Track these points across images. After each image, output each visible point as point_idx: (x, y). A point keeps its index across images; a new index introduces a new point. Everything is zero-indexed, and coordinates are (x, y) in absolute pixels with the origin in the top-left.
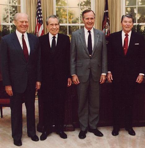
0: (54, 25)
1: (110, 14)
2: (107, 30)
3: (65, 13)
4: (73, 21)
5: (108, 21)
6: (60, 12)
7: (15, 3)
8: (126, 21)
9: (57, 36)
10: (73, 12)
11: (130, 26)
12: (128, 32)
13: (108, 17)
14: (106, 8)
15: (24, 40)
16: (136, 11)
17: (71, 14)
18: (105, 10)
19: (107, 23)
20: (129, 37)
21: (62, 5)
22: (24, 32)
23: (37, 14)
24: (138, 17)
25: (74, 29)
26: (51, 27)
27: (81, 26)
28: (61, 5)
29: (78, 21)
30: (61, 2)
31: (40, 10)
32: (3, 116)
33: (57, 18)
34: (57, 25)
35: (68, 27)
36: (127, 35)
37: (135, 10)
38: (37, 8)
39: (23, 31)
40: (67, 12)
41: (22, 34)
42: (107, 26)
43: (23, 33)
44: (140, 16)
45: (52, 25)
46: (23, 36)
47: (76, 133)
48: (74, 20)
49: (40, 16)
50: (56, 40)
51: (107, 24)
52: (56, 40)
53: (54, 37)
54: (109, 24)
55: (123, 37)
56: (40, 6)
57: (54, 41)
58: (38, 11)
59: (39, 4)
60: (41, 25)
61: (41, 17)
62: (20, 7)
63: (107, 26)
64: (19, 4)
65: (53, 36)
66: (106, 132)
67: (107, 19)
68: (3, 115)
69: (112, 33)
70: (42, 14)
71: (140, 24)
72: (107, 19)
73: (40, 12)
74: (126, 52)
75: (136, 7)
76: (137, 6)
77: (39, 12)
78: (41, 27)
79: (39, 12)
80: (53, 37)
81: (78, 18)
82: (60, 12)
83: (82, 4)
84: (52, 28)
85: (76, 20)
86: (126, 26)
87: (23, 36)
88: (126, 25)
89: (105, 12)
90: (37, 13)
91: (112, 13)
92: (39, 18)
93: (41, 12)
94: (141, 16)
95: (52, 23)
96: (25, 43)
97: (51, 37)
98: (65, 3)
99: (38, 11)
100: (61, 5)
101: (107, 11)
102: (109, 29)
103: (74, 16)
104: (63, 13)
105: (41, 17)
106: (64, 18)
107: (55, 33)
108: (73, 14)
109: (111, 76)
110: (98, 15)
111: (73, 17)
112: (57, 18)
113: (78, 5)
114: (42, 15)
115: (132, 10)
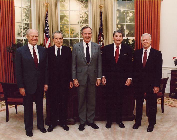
0: (59, 39)
1: (104, 30)
2: (101, 43)
3: (67, 29)
5: (103, 36)
7: (27, 21)
9: (61, 48)
10: (74, 29)
12: (119, 44)
13: (102, 32)
14: (101, 25)
16: (125, 28)
17: (72, 30)
18: (100, 27)
19: (102, 37)
20: (120, 49)
21: (65, 23)
22: (35, 45)
23: (45, 30)
24: (126, 32)
26: (57, 41)
28: (65, 22)
29: (78, 36)
31: (47, 27)
33: (62, 33)
34: (61, 39)
36: (118, 47)
38: (45, 25)
39: (34, 43)
41: (32, 46)
42: (101, 39)
43: (34, 45)
44: (128, 32)
45: (57, 39)
46: (34, 47)
47: (77, 126)
48: (75, 35)
49: (47, 31)
50: (60, 51)
51: (101, 38)
52: (60, 51)
53: (59, 49)
54: (103, 38)
55: (115, 49)
56: (47, 24)
59: (47, 22)
62: (31, 24)
63: (101, 39)
65: (58, 48)
66: (101, 125)
67: (102, 34)
70: (49, 30)
72: (102, 34)
73: (47, 28)
74: (117, 61)
75: (125, 25)
76: (126, 24)
77: (46, 28)
78: (48, 41)
79: (46, 28)
80: (58, 49)
83: (81, 22)
86: (117, 40)
87: (34, 47)
89: (100, 28)
90: (45, 29)
91: (105, 30)
92: (46, 33)
93: (48, 28)
95: (57, 37)
98: (68, 21)
101: (102, 27)
102: (103, 42)
103: (75, 32)
104: (66, 29)
106: (67, 33)
107: (59, 46)
108: (74, 30)
109: (105, 80)
111: (74, 32)
113: (78, 23)
114: (49, 31)
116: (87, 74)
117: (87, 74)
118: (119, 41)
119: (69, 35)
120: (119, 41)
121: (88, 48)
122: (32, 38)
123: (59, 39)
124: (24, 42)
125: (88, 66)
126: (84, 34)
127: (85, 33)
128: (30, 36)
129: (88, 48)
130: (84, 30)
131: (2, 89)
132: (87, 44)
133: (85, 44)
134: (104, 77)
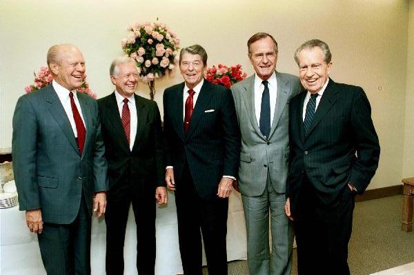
36: (191, 93)
55: (186, 96)
116: (265, 166)
117: (265, 166)
118: (194, 75)
120: (194, 75)
121: (266, 94)
122: (71, 69)
123: (309, 67)
124: (209, 75)
125: (268, 144)
126: (253, 57)
127: (258, 52)
128: (65, 64)
129: (266, 94)
130: (254, 45)
131: (192, 173)
132: (265, 83)
133: (258, 81)
134: (171, 167)
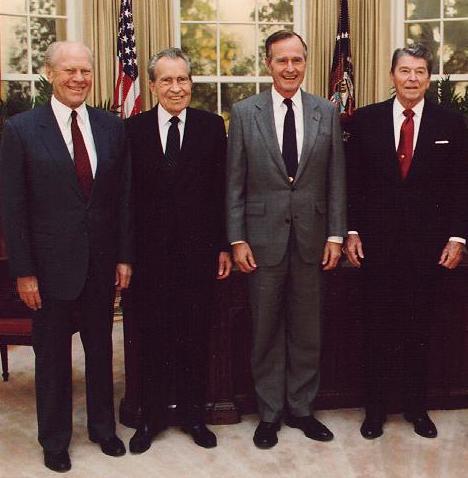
0: (175, 82)
1: (355, 46)
2: (344, 96)
3: (209, 41)
4: (236, 66)
5: (349, 67)
6: (192, 40)
7: (48, 10)
8: (406, 68)
9: (183, 117)
10: (236, 39)
11: (421, 85)
12: (414, 102)
13: (348, 53)
14: (343, 25)
15: (78, 128)
16: (438, 36)
17: (229, 45)
18: (339, 32)
19: (346, 73)
20: (417, 120)
21: (200, 16)
22: (78, 105)
23: (121, 46)
24: (444, 54)
25: (240, 94)
26: (166, 88)
27: (261, 84)
28: (198, 15)
29: (250, 68)
30: (196, 7)
31: (129, 33)
32: (11, 376)
33: (185, 57)
34: (183, 79)
35: (219, 86)
36: (409, 114)
37: (435, 31)
38: (120, 25)
39: (75, 99)
40: (216, 40)
41: (69, 111)
42: (344, 83)
43: (74, 106)
44: (452, 52)
45: (169, 80)
46: (74, 115)
48: (238, 65)
49: (128, 51)
50: (181, 128)
51: (345, 77)
52: (181, 128)
53: (175, 121)
54: (352, 78)
55: (398, 120)
56: (128, 20)
57: (173, 131)
58: (121, 36)
59: (127, 13)
60: (134, 79)
61: (133, 56)
62: (64, 22)
63: (344, 83)
64: (62, 14)
65: (170, 116)
66: (344, 427)
67: (346, 62)
68: (9, 371)
69: (361, 106)
70: (134, 45)
71: (453, 77)
72: (345, 60)
73: (129, 38)
74: (405, 169)
75: (438, 24)
76: (442, 19)
77: (125, 39)
78: (132, 87)
79: (125, 39)
80: (170, 121)
81: (251, 58)
82: (192, 40)
83: (265, 14)
84: (169, 90)
85: (244, 65)
86: (408, 84)
87: (74, 115)
88: (405, 82)
89: (339, 38)
90: (119, 41)
91: (360, 44)
92: (125, 57)
93: (133, 38)
94: (455, 53)
95: (169, 73)
96: (82, 138)
97: (164, 119)
98: (209, 8)
99: (121, 36)
100: (198, 15)
101: (346, 35)
102: (352, 93)
103: (238, 52)
104: (205, 43)
105: (133, 56)
106: (208, 57)
107: (177, 107)
108: (237, 44)
110: (316, 49)
111: (235, 55)
112: (185, 57)
113: (253, 15)
114: (134, 49)
115: (427, 32)
119: (214, 65)
